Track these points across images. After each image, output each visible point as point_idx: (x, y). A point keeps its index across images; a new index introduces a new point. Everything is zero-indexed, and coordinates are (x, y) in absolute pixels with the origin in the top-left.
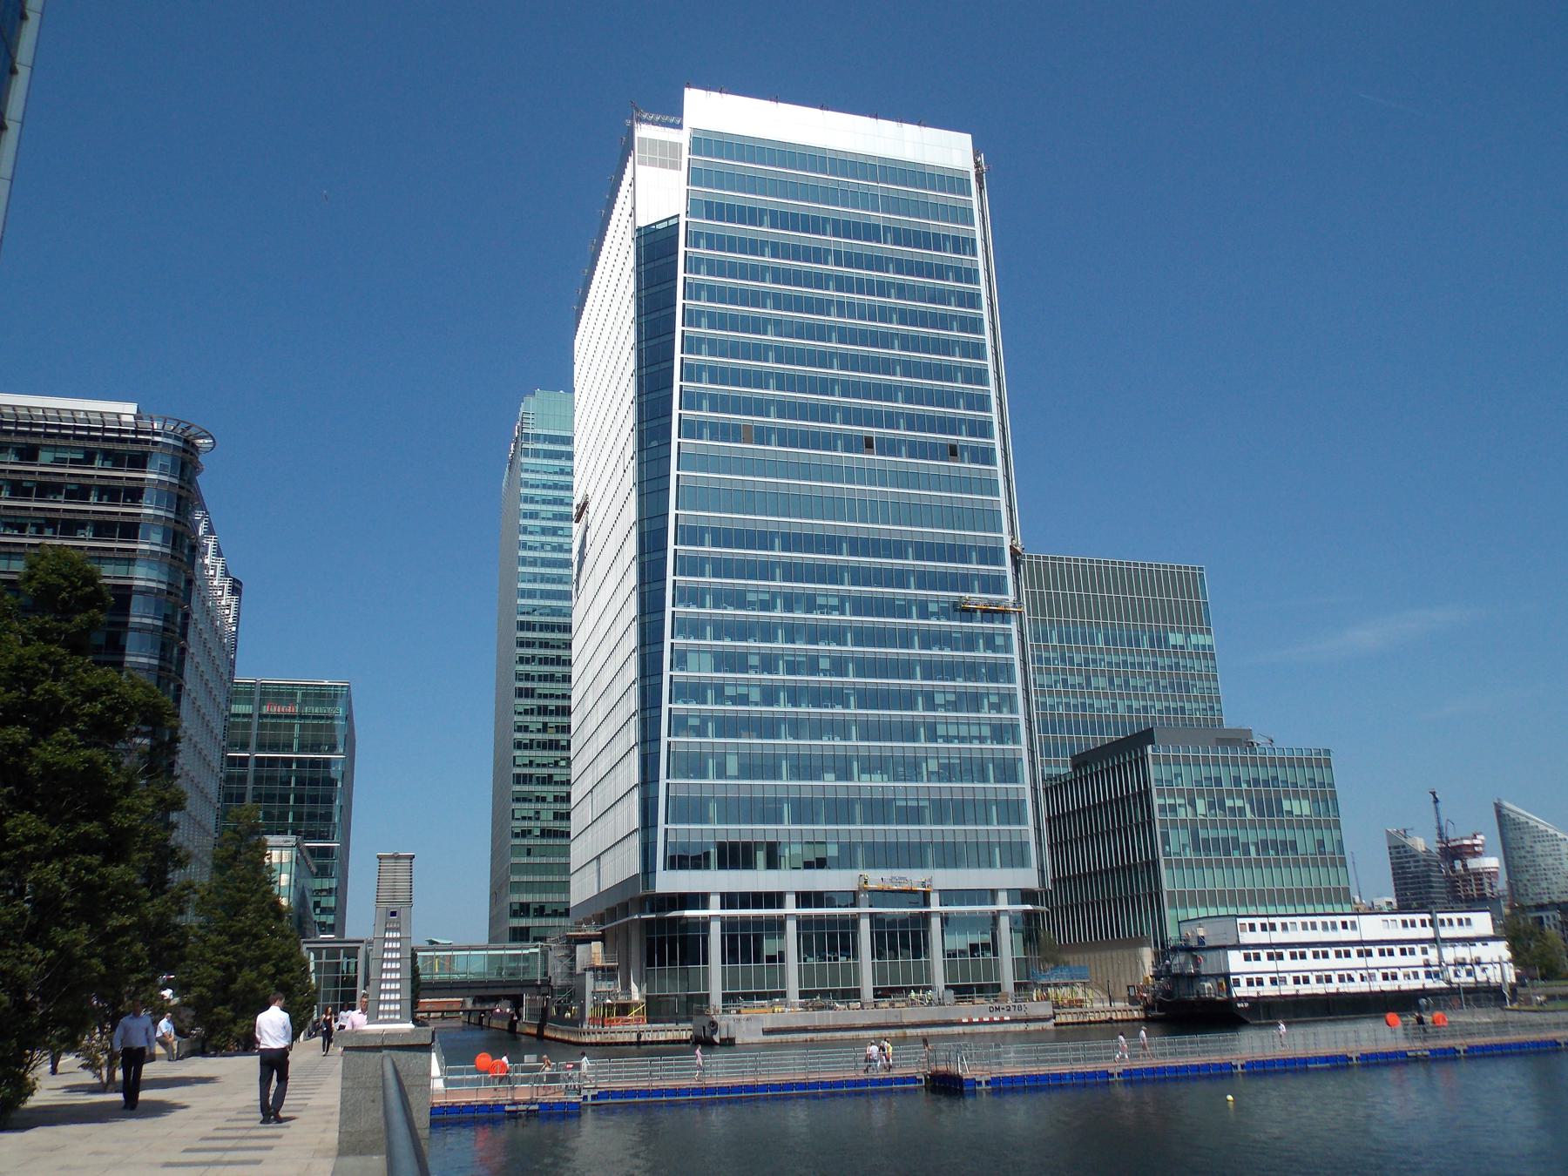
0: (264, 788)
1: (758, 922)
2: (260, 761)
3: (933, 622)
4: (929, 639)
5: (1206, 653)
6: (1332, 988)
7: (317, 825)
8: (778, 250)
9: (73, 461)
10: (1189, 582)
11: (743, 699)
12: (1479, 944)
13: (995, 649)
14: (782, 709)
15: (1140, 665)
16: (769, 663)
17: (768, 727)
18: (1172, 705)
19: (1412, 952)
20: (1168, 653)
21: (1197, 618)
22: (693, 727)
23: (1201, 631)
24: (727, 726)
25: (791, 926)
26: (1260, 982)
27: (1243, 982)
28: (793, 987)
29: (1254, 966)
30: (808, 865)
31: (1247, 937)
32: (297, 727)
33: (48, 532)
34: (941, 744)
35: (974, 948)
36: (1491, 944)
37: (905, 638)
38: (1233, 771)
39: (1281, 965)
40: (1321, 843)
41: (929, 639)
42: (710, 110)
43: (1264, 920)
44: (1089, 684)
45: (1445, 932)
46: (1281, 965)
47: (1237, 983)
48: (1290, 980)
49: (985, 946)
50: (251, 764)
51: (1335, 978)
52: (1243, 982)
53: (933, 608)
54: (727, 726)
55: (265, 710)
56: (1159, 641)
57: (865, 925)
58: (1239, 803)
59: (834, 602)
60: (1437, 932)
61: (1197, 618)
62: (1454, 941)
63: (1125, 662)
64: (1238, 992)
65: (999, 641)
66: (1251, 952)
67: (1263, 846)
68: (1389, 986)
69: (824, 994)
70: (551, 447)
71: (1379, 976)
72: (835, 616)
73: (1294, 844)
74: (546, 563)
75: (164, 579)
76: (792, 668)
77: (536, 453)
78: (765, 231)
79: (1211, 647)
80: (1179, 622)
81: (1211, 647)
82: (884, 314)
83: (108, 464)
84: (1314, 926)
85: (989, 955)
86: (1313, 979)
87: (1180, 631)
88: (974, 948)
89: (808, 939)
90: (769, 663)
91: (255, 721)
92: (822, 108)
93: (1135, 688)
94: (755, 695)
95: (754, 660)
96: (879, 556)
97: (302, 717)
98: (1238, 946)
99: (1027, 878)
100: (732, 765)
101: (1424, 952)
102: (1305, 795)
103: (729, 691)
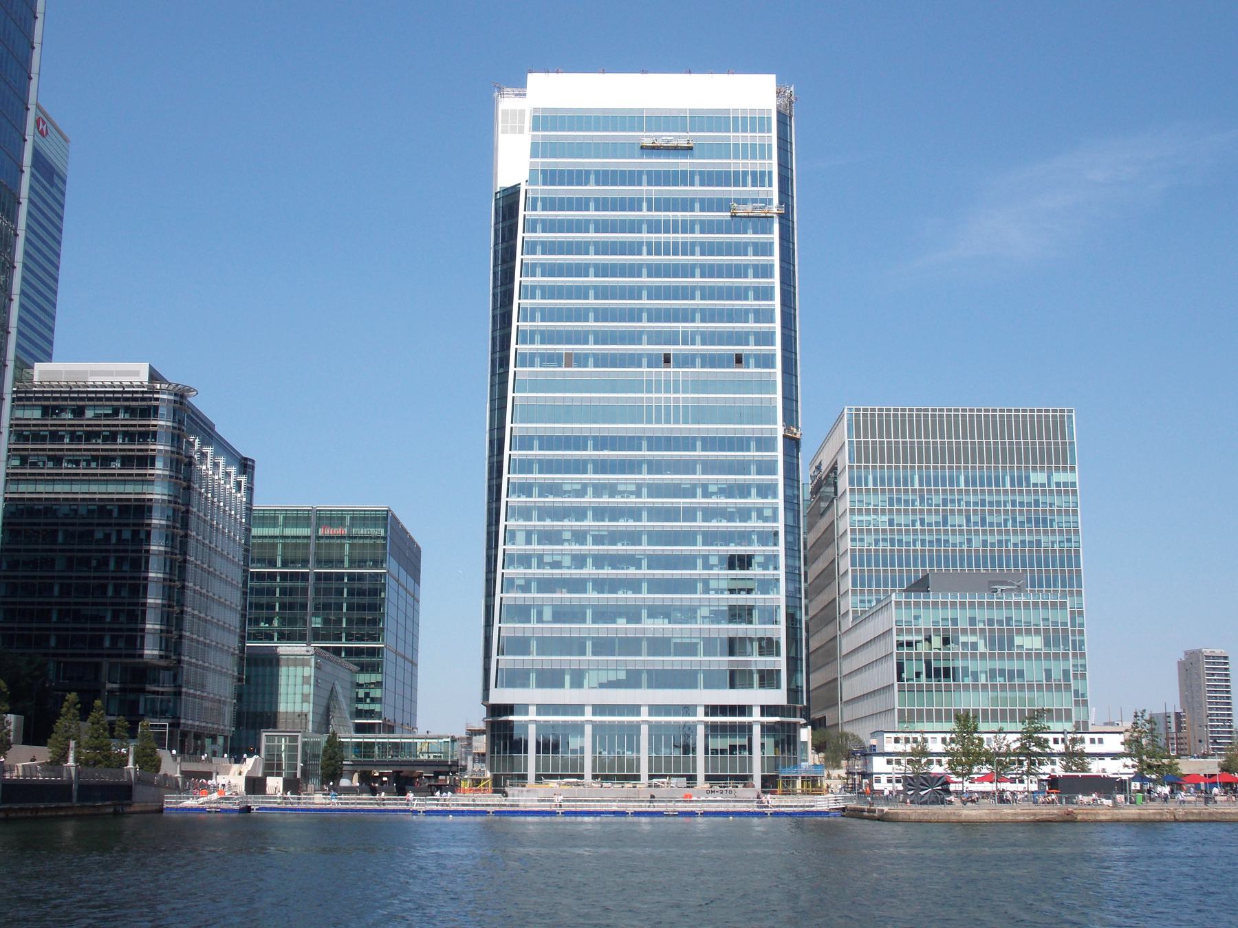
0: (322, 599)
1: (565, 725)
2: (318, 575)
3: (714, 500)
4: (710, 513)
5: (1067, 489)
7: (366, 629)
8: (602, 204)
9: (106, 415)
10: (1057, 425)
11: (556, 565)
12: (1108, 759)
13: (766, 519)
14: (589, 571)
15: (998, 503)
16: (579, 537)
17: (576, 585)
18: (1027, 538)
20: (1028, 492)
21: (1060, 457)
22: (518, 586)
23: (1065, 469)
24: (547, 585)
25: (588, 729)
27: (884, 778)
28: (531, 773)
30: (602, 686)
32: (347, 547)
33: (93, 465)
34: (712, 595)
35: (733, 748)
37: (690, 514)
38: (968, 613)
40: (1048, 673)
41: (710, 513)
42: (551, 90)
44: (945, 523)
47: (878, 780)
49: (742, 747)
50: (311, 579)
52: (884, 778)
53: (713, 489)
54: (547, 585)
55: (321, 532)
56: (1021, 481)
57: (644, 730)
58: (972, 639)
59: (633, 488)
61: (1060, 457)
63: (983, 501)
65: (768, 513)
67: (992, 674)
69: (724, 778)
72: (633, 499)
73: (1021, 674)
75: (166, 492)
76: (598, 540)
78: (592, 189)
79: (1073, 484)
80: (1042, 462)
81: (1073, 484)
82: (688, 248)
83: (127, 416)
85: (746, 754)
87: (1042, 469)
88: (733, 748)
89: (602, 739)
90: (579, 537)
91: (312, 542)
92: (643, 72)
93: (991, 524)
94: (567, 561)
95: (567, 535)
96: (670, 450)
97: (350, 538)
99: (778, 697)
100: (547, 614)
102: (1037, 632)
103: (547, 559)
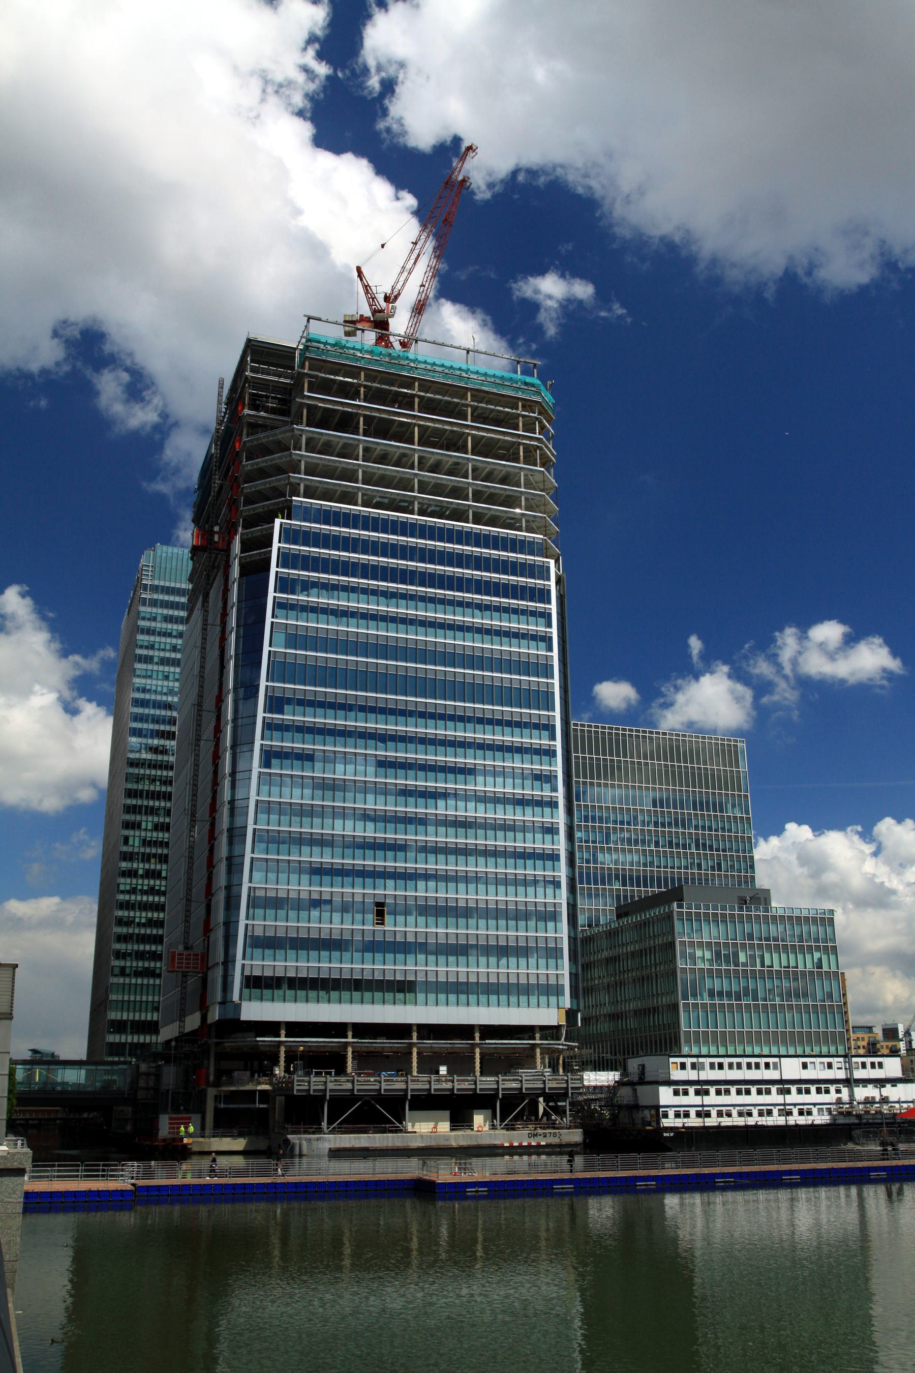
6: (751, 1121)
12: (888, 1086)
19: (827, 1091)
26: (687, 1115)
27: (671, 1113)
29: (682, 1100)
31: (677, 1074)
36: (900, 1086)
39: (707, 1100)
43: (694, 1060)
45: (859, 1074)
46: (789, 1099)
47: (666, 1116)
48: (714, 1113)
51: (755, 1112)
52: (671, 1113)
60: (852, 1074)
62: (865, 1082)
64: (666, 1123)
66: (681, 1088)
68: (802, 1120)
70: (166, 598)
71: (795, 1111)
74: (143, 939)
77: (154, 603)
84: (757, 1066)
86: (734, 1112)
98: (669, 1083)
101: (838, 1091)
